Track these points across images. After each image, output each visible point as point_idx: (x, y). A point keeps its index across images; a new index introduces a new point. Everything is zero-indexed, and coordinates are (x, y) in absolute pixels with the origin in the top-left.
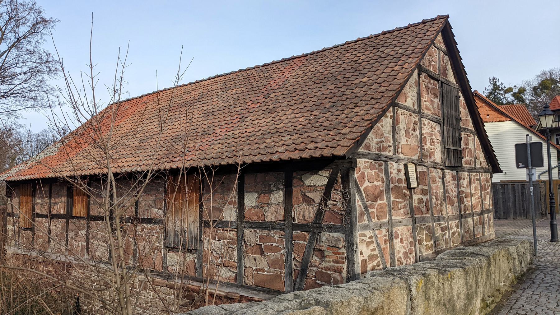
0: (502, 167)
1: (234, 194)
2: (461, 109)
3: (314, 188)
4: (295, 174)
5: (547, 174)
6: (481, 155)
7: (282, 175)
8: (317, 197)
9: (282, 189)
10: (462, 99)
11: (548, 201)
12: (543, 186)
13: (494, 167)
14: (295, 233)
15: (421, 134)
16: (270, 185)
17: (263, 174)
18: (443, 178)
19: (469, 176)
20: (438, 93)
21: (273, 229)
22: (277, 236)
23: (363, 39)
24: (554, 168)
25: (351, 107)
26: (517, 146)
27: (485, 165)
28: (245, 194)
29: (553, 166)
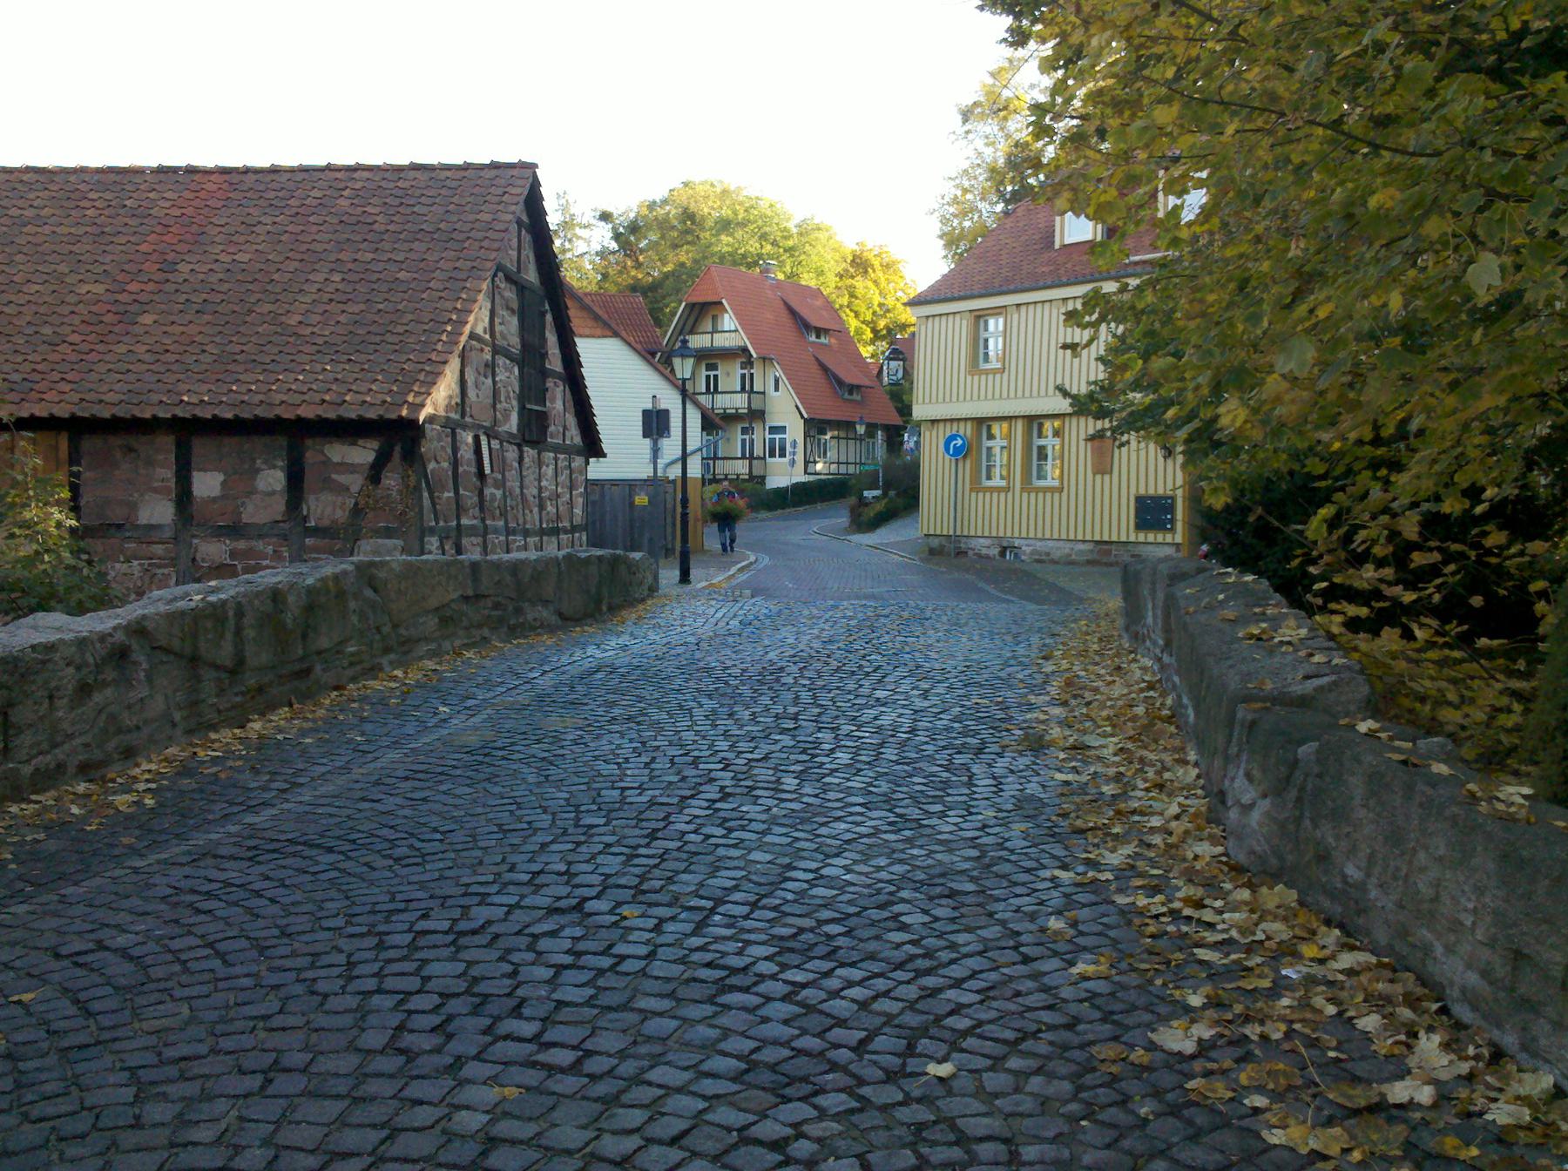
0: (605, 447)
2: (548, 334)
3: (351, 468)
4: (309, 442)
5: (679, 466)
6: (571, 421)
7: (282, 441)
8: (355, 482)
9: (281, 469)
10: (549, 318)
11: (679, 510)
12: (670, 488)
13: (592, 446)
15: (494, 383)
16: (253, 460)
17: (236, 439)
19: (556, 459)
20: (515, 306)
22: (270, 549)
23: (370, 168)
26: (534, 166)
27: (578, 440)
28: (195, 474)
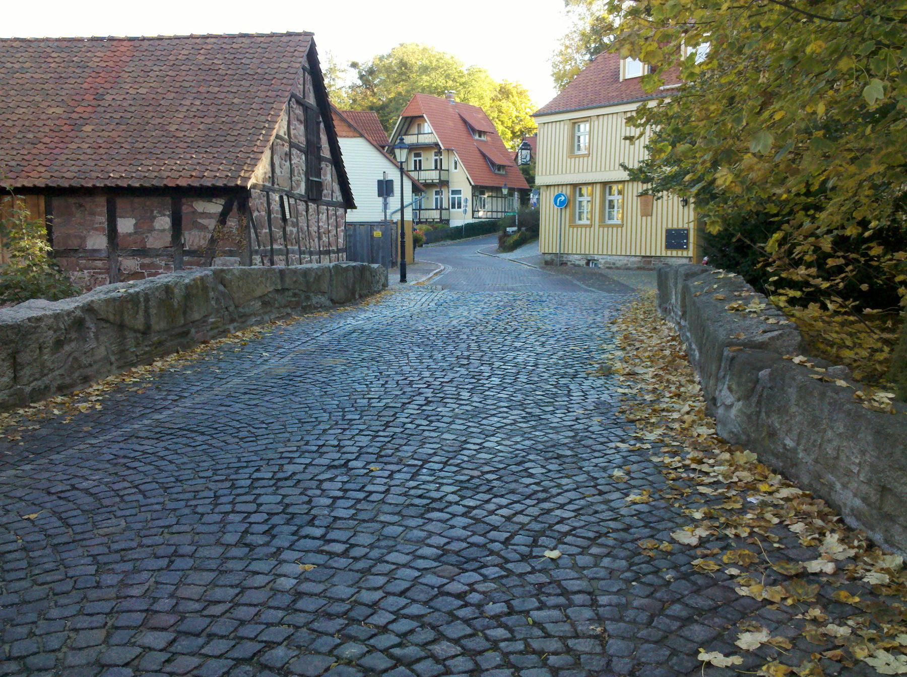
0: (356, 203)
1: (102, 219)
4: (184, 200)
6: (336, 187)
7: (169, 200)
8: (212, 224)
10: (322, 125)
12: (394, 226)
13: (348, 202)
14: (186, 259)
15: (291, 165)
16: (152, 211)
17: (142, 199)
18: (307, 211)
19: (327, 210)
20: (302, 119)
21: (157, 256)
24: (407, 206)
25: (18, 136)
27: (340, 199)
29: (405, 204)
